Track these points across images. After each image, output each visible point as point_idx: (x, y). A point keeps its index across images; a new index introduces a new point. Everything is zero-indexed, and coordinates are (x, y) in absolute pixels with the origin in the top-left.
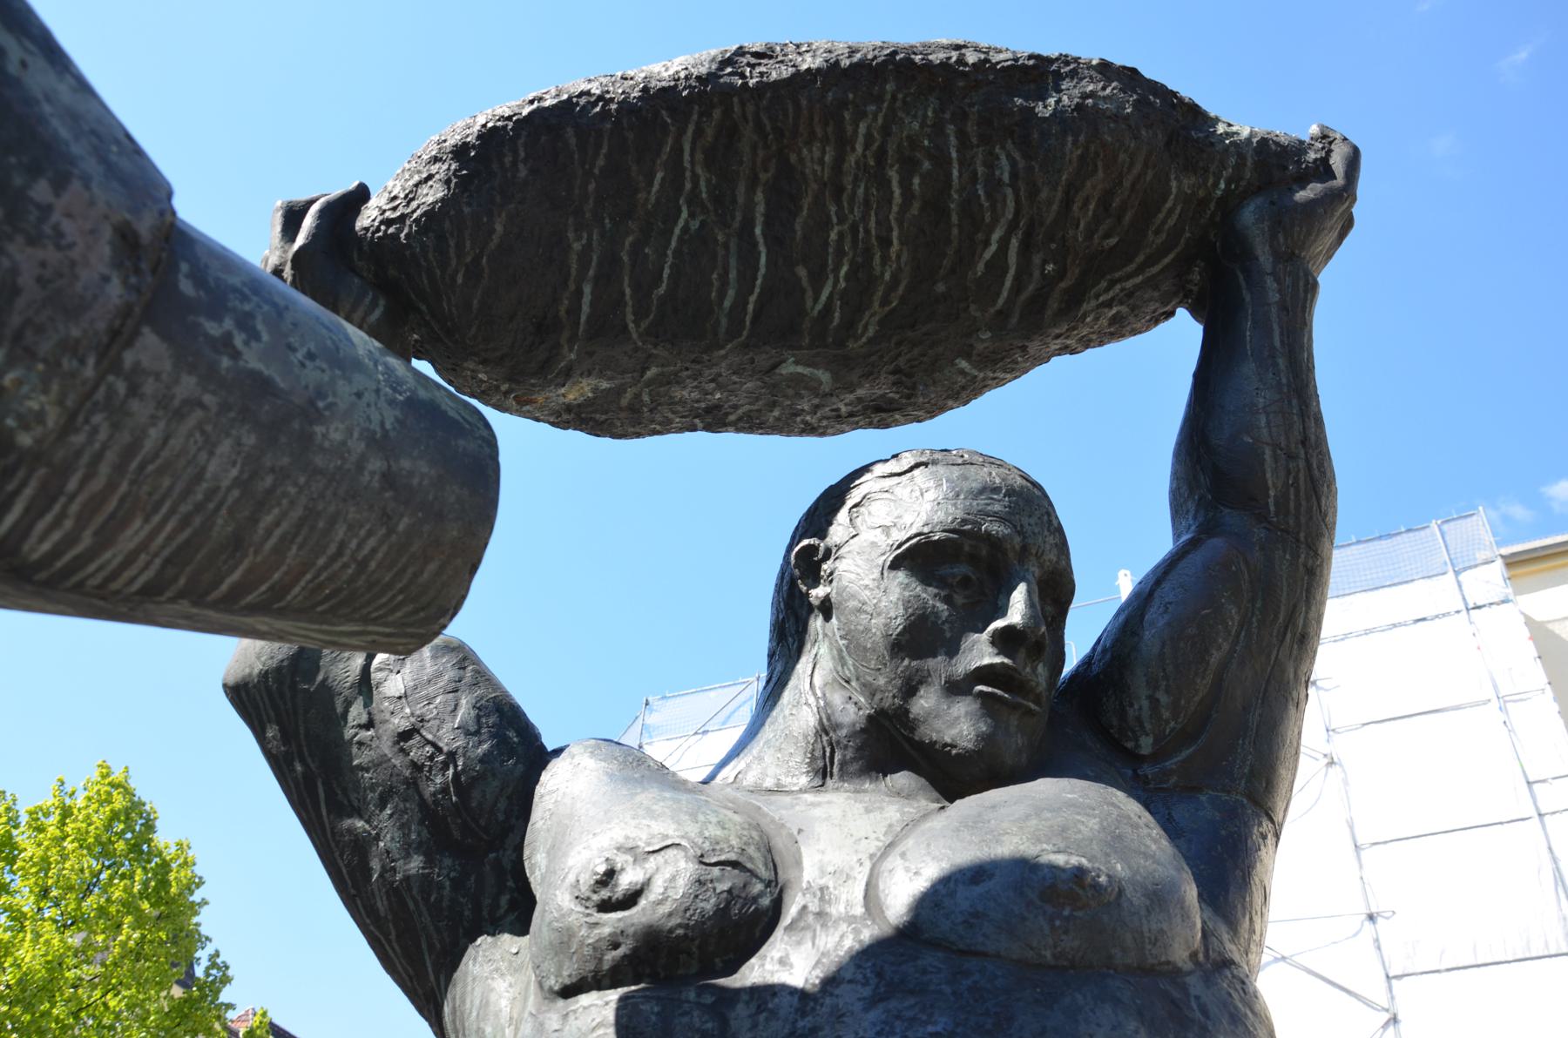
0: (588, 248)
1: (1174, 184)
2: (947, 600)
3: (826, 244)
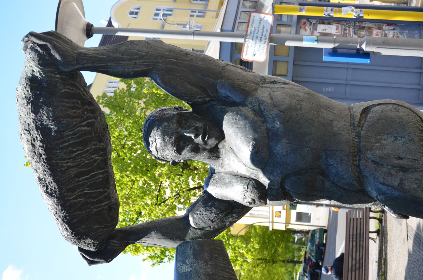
0: (95, 208)
1: (63, 91)
2: (188, 145)
3: (89, 162)
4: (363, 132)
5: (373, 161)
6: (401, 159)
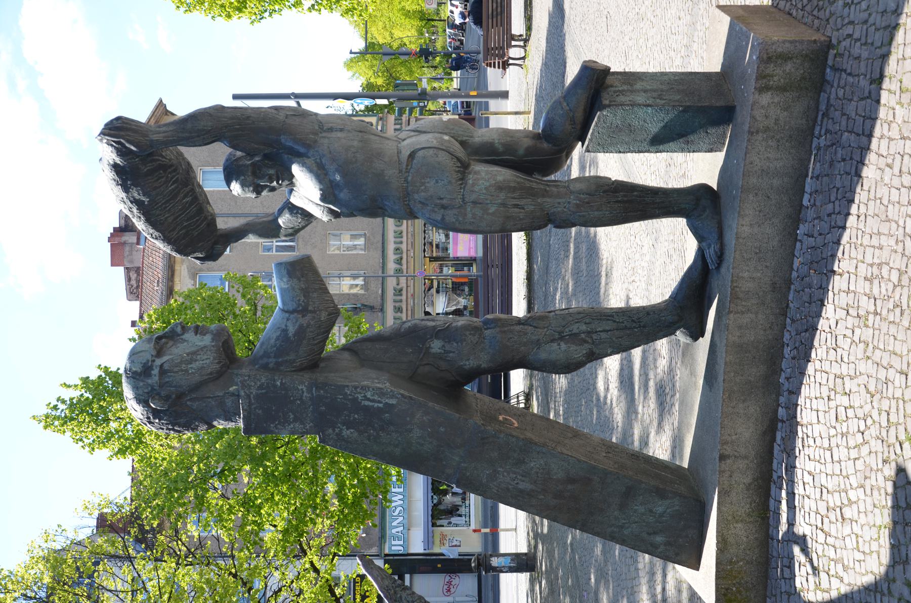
4: (410, 178)
5: (420, 202)
6: (441, 199)
